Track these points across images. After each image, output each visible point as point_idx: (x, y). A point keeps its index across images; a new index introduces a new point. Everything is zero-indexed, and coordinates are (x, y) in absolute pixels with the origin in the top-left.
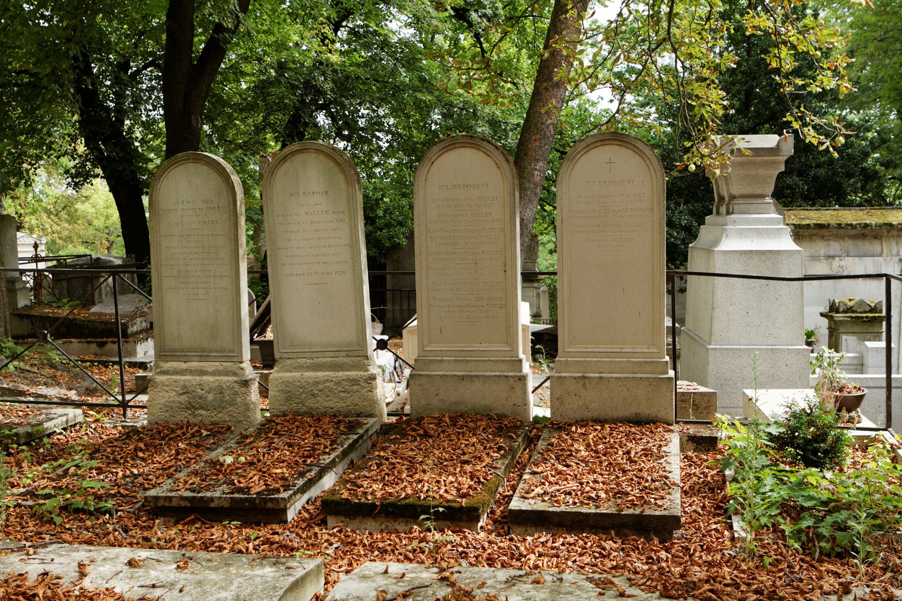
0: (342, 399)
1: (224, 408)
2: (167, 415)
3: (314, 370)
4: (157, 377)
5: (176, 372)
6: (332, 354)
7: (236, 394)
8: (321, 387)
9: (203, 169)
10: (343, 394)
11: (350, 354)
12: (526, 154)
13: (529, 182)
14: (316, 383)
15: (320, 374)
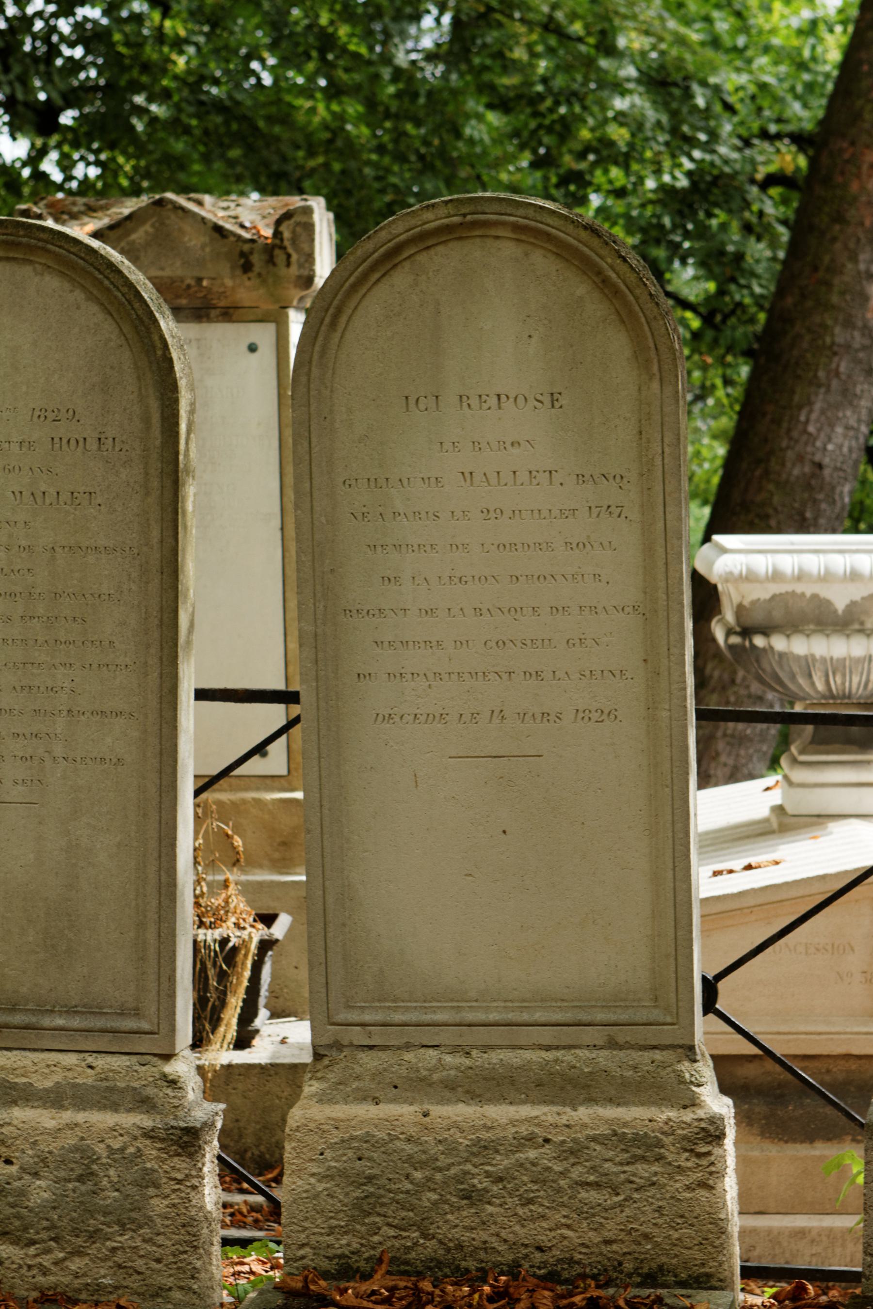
0: (586, 1212)
1: (94, 1236)
3: (474, 1096)
6: (547, 1035)
8: (502, 1162)
9: (45, 286)
10: (592, 1196)
11: (622, 1035)
12: (839, 218)
13: (849, 324)
14: (484, 1149)
15: (500, 1113)
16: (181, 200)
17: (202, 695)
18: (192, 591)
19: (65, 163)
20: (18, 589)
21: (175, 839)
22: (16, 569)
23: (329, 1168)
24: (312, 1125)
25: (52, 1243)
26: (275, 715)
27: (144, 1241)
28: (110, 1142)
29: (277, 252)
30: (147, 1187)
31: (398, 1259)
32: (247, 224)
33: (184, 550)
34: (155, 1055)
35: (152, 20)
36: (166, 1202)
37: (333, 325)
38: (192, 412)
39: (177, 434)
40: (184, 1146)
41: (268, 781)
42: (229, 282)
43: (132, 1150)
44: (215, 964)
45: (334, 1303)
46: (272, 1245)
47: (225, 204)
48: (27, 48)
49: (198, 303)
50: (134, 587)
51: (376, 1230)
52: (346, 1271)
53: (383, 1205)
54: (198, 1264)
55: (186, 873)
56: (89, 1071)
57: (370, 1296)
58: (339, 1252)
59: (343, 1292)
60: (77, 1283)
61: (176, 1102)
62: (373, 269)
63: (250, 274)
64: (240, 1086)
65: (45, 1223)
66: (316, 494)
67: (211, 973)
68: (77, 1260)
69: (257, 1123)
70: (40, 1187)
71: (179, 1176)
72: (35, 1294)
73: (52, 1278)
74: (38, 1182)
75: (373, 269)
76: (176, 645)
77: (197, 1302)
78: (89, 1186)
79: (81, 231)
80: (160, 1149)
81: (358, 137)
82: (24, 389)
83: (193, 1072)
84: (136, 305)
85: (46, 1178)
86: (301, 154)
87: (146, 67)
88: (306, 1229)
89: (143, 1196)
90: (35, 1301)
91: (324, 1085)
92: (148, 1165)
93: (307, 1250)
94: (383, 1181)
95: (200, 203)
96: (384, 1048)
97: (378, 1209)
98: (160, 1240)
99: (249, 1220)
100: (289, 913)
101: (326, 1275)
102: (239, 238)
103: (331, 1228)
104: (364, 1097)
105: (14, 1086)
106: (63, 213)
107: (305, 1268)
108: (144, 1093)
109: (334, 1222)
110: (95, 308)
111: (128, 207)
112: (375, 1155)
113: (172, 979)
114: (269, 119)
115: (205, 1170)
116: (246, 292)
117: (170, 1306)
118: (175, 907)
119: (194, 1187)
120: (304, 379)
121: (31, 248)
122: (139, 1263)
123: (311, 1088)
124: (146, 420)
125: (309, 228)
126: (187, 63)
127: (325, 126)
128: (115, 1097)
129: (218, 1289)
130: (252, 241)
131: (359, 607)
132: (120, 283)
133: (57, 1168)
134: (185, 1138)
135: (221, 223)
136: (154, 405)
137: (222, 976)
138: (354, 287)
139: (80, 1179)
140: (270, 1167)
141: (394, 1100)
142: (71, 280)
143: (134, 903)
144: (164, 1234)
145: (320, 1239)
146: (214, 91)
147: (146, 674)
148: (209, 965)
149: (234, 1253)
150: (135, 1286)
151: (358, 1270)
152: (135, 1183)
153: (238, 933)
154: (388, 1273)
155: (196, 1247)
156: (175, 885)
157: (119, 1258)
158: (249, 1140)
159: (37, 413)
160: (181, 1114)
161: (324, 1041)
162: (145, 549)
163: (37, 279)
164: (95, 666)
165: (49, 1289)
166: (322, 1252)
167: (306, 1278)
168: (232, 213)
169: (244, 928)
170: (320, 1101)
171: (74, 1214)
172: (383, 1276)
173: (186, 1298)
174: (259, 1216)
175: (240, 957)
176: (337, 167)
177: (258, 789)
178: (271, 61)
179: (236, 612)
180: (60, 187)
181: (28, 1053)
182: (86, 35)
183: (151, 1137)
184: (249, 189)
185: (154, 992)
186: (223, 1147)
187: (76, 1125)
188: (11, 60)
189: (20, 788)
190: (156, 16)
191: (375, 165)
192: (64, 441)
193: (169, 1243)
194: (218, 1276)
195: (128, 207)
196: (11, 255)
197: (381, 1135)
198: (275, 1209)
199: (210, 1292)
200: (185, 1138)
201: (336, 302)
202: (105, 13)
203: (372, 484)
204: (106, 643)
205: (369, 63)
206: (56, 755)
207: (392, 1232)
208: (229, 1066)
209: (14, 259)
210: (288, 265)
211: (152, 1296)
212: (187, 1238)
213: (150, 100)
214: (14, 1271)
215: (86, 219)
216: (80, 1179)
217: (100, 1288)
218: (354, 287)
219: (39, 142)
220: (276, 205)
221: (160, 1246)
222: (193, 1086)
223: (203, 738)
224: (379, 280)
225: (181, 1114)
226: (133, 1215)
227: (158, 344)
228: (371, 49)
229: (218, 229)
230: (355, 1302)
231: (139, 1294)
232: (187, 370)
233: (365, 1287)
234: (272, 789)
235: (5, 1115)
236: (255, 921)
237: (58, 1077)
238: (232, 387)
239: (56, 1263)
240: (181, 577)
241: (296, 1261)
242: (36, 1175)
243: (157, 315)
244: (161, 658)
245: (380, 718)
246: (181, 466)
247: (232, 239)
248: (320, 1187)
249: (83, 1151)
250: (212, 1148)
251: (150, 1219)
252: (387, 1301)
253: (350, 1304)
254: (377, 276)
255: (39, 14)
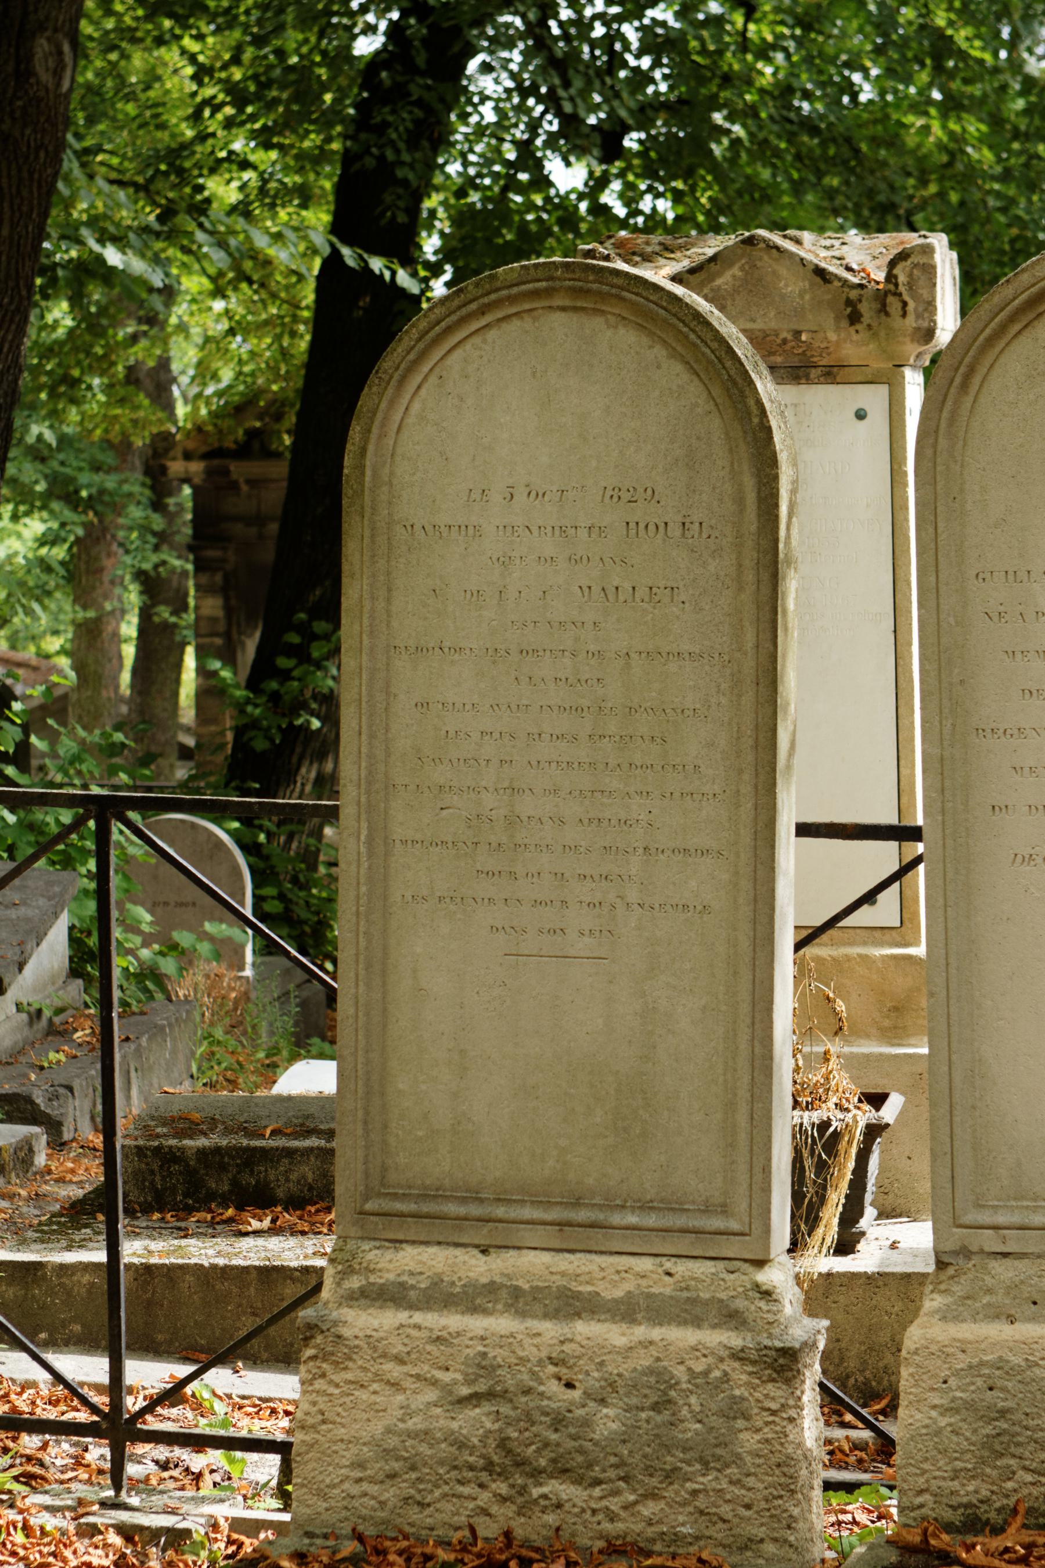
1: (670, 1475)
2: (390, 1494)
4: (348, 1314)
5: (440, 1296)
7: (736, 1410)
9: (618, 341)
16: (776, 238)
17: (804, 830)
18: (792, 707)
19: (630, 194)
20: (585, 703)
21: (771, 1002)
22: (583, 678)
23: (953, 1400)
24: (934, 1348)
25: (621, 1484)
26: (885, 856)
27: (731, 1482)
28: (690, 1363)
29: (890, 299)
30: (735, 1418)
31: (1036, 1510)
32: (855, 267)
33: (784, 656)
34: (745, 1261)
35: (733, 24)
36: (757, 1437)
37: (965, 386)
38: (794, 492)
39: (776, 518)
40: (780, 1370)
41: (878, 934)
42: (832, 336)
43: (717, 1373)
44: (812, 1153)
45: (958, 1561)
46: (884, 1491)
47: (828, 243)
48: (586, 56)
49: (795, 361)
50: (724, 701)
51: (1011, 1475)
52: (973, 1524)
53: (1018, 1444)
54: (796, 1512)
55: (784, 1043)
56: (667, 1278)
57: (1001, 1554)
58: (965, 1500)
59: (970, 1548)
60: (650, 1532)
61: (770, 1317)
62: (1012, 319)
63: (858, 327)
64: (842, 1299)
65: (613, 1460)
66: (943, 589)
67: (808, 1163)
68: (651, 1504)
69: (862, 1343)
70: (607, 1416)
71: (774, 1406)
72: (600, 1544)
73: (620, 1526)
74: (605, 1411)
75: (1012, 319)
76: (774, 770)
77: (794, 1557)
78: (666, 1415)
79: (659, 274)
80: (750, 1374)
81: (979, 161)
82: (594, 463)
83: (791, 1282)
84: (728, 364)
85: (614, 1405)
86: (911, 181)
87: (727, 79)
88: (924, 1472)
89: (730, 1429)
90: (601, 1552)
91: (949, 1299)
92: (737, 1392)
93: (926, 1497)
94: (1019, 1416)
95: (798, 242)
96: (1022, 1256)
97: (1012, 1449)
98: (751, 1481)
99: (852, 1459)
100: (902, 1093)
101: (949, 1528)
102: (845, 281)
103: (955, 1471)
104: (998, 1314)
105: (577, 1296)
106: (634, 254)
107: (924, 1519)
108: (733, 1306)
109: (959, 1464)
110: (678, 367)
111: (713, 245)
112: (1010, 1385)
113: (767, 1170)
114: (875, 142)
115: (805, 1398)
116: (853, 347)
117: (761, 1561)
118: (771, 1084)
119: (791, 1420)
120: (929, 452)
121: (602, 296)
122: (725, 1510)
123: (933, 1302)
124: (740, 501)
125: (930, 271)
126: (774, 74)
127: (941, 146)
128: (698, 1310)
129: (818, 1542)
130: (861, 286)
131: (994, 725)
132: (708, 337)
133: (628, 1394)
134: (781, 1361)
135: (823, 265)
136: (749, 483)
137: (821, 1167)
138: (990, 341)
139: (656, 1407)
140: (877, 1396)
141: (1033, 1319)
142: (651, 334)
143: (721, 1079)
144: (755, 1475)
145: (942, 1484)
146: (806, 106)
147: (738, 806)
148: (806, 1154)
149: (837, 1499)
150: (720, 1536)
151: (987, 1522)
152: (721, 1414)
153: (840, 1116)
154: (1025, 1526)
155: (793, 1492)
156: (771, 1058)
157: (701, 1502)
158: (852, 1364)
159: (609, 493)
160: (776, 1331)
161: (949, 1246)
162: (738, 655)
163: (609, 333)
164: (677, 795)
165: (617, 1538)
166: (945, 1500)
167: (925, 1532)
168: (837, 254)
169: (847, 1110)
170: (944, 1318)
171: (648, 1450)
172: (1018, 1530)
173: (781, 1553)
174: (863, 1455)
175: (842, 1145)
176: (954, 197)
177: (865, 943)
178: (874, 72)
179: (846, 728)
180: (623, 224)
181: (594, 1257)
182: (656, 43)
183: (741, 1359)
184: (848, 224)
185: (745, 1186)
186: (824, 1372)
187: (651, 1343)
188: (571, 72)
189: (587, 940)
190: (739, 19)
191: (998, 195)
192: (642, 526)
193: (761, 1486)
194: (819, 1526)
195: (713, 245)
196: (579, 304)
197: (1016, 1360)
198: (886, 1447)
199: (809, 1545)
200: (781, 1361)
201: (967, 360)
202: (678, 15)
203: (1011, 577)
204: (690, 768)
205: (996, 70)
206: (630, 900)
207: (1029, 1478)
208: (829, 1275)
209: (583, 309)
210: (904, 315)
211: (740, 1549)
212: (783, 1480)
213: (729, 118)
214: (576, 1515)
215: (662, 261)
216: (656, 1407)
217: (677, 1538)
218: (990, 341)
219: (598, 170)
220: (890, 242)
221: (749, 1489)
222: (790, 1300)
223: (806, 881)
224: (1020, 332)
225: (776, 1331)
226: (718, 1451)
227: (755, 410)
228: (996, 55)
229: (820, 273)
230: (983, 1560)
231: (724, 1546)
232: (788, 442)
233: (997, 1543)
234: (882, 944)
235: (566, 1330)
236: (860, 1101)
237: (629, 1286)
238: (843, 459)
239: (625, 1508)
240: (780, 689)
241: (913, 1509)
242: (603, 1402)
243: (753, 375)
244: (756, 786)
245: (1019, 858)
246: (781, 556)
247: (837, 284)
248: (943, 1422)
249: (659, 1374)
250: (813, 1373)
251: (739, 1456)
252: (1023, 1560)
253: (978, 1562)
254: (1017, 327)
255: (600, 16)
